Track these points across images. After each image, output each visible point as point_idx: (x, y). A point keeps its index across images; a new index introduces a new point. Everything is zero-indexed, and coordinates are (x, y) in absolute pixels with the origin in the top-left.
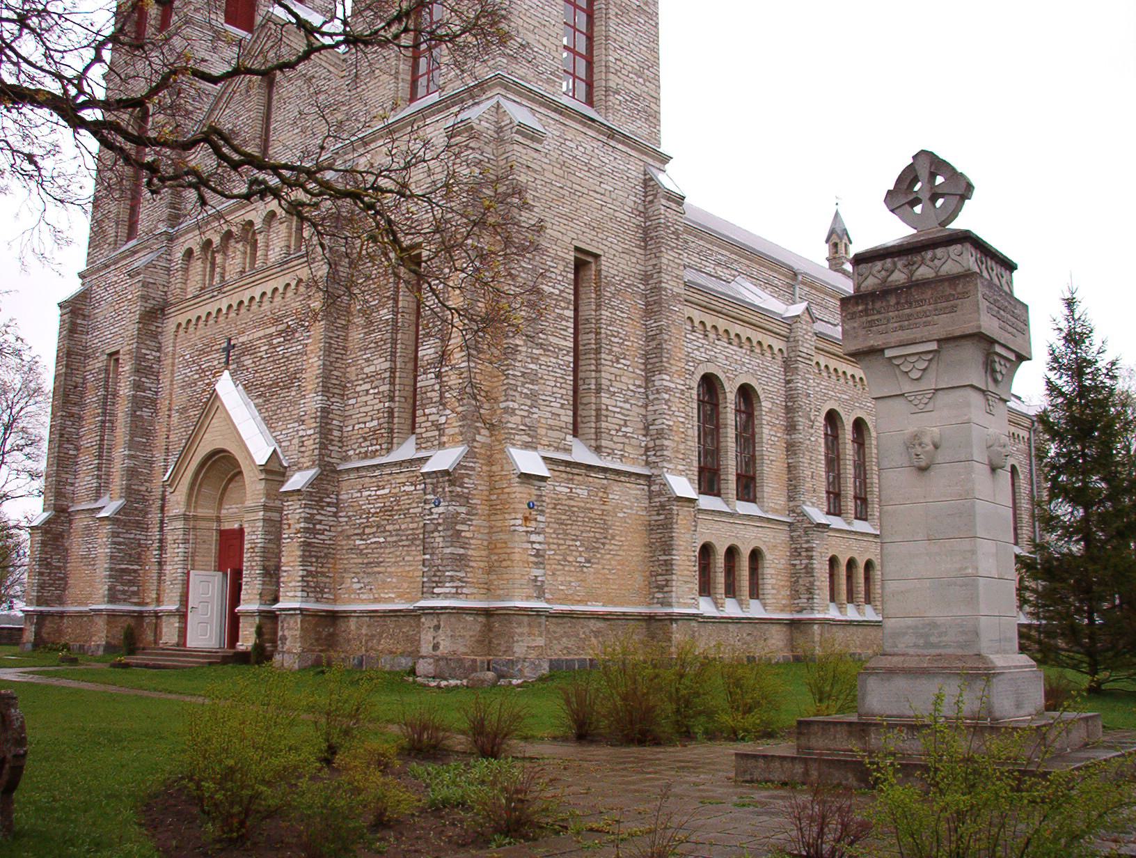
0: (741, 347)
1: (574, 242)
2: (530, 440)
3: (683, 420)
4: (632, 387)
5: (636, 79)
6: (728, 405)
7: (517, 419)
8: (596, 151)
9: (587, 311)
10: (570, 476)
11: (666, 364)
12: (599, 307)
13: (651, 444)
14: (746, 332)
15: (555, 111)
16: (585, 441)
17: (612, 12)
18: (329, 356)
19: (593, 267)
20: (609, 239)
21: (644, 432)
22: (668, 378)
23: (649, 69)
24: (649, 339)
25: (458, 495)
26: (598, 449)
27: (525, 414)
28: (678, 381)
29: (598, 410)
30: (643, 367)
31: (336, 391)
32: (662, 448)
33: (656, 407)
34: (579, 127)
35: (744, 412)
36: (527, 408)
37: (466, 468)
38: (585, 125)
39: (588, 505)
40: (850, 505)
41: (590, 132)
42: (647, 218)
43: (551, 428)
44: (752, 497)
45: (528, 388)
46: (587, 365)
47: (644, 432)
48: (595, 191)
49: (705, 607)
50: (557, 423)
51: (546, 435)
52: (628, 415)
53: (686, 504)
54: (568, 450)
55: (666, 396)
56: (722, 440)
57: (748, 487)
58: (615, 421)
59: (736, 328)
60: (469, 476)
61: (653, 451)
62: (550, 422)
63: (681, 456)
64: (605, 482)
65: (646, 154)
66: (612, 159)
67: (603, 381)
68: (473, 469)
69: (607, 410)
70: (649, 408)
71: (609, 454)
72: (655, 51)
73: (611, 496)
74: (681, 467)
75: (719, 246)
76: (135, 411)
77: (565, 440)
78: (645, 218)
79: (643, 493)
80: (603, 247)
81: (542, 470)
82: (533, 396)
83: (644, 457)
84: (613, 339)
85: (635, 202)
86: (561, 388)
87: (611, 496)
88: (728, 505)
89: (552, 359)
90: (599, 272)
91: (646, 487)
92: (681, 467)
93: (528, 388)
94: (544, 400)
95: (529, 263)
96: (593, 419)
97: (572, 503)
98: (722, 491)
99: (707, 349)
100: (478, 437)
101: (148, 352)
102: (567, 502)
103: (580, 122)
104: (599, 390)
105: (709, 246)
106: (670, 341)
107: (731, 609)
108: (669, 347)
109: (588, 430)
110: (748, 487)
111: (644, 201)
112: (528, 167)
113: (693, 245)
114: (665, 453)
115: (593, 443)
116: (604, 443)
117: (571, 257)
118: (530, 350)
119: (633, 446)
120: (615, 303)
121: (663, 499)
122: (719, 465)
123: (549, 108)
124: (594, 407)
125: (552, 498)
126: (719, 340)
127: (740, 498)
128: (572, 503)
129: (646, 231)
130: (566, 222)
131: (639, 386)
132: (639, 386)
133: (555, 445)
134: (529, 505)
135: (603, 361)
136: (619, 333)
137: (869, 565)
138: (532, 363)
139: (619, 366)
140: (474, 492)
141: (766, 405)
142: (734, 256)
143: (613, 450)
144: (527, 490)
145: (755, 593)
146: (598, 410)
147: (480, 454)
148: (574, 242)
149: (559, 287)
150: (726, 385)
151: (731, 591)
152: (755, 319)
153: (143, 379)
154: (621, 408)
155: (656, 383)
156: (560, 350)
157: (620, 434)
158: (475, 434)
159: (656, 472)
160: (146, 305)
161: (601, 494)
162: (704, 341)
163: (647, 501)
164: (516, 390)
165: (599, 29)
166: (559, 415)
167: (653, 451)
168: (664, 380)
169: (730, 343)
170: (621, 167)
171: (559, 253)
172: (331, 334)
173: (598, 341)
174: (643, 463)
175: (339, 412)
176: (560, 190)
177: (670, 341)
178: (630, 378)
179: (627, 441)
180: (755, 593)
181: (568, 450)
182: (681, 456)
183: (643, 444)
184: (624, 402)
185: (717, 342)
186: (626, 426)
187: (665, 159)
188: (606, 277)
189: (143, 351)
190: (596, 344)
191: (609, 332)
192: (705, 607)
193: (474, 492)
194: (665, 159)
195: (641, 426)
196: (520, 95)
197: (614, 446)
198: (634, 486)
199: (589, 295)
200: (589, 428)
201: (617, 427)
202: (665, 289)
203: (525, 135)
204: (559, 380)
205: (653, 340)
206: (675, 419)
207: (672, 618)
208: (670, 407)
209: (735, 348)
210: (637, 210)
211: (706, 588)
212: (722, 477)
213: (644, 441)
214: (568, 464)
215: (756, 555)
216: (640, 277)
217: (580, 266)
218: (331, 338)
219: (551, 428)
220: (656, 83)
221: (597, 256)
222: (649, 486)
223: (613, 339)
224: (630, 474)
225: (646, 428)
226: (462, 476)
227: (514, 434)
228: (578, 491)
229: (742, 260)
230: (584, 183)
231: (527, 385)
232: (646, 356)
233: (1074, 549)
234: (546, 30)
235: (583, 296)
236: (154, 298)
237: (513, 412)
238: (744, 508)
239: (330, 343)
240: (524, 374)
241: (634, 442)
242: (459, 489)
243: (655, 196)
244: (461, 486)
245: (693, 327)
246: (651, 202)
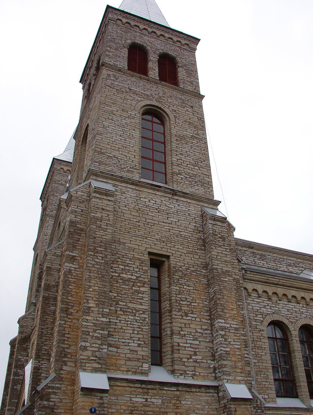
0: (299, 303)
1: (147, 250)
2: (100, 366)
3: (239, 347)
4: (199, 331)
5: (193, 167)
6: (294, 338)
8: (163, 202)
10: (146, 391)
11: (220, 313)
13: (217, 366)
14: (299, 294)
15: (132, 184)
17: (174, 140)
18: (41, 338)
19: (166, 263)
20: (176, 247)
21: (212, 358)
22: (223, 321)
25: (44, 407)
26: (173, 372)
27: (97, 349)
28: (232, 322)
30: (209, 318)
31: (44, 357)
32: (221, 366)
33: (217, 341)
34: (151, 191)
35: (306, 342)
36: (97, 346)
37: (53, 388)
38: (154, 190)
39: (162, 410)
41: (158, 193)
44: (295, 395)
45: (99, 333)
47: (212, 358)
48: (164, 222)
50: (135, 356)
51: (125, 364)
52: (196, 348)
53: (243, 403)
55: (223, 333)
56: (293, 360)
58: (185, 352)
59: (291, 293)
60: (55, 393)
62: (128, 356)
63: (239, 371)
64: (178, 393)
65: (202, 201)
66: (177, 205)
67: (174, 328)
68: (60, 388)
69: (179, 345)
70: (215, 342)
71: (181, 374)
73: (183, 402)
74: (239, 378)
75: (287, 256)
76: (13, 387)
77: (142, 367)
78: (204, 234)
79: (213, 398)
80: (171, 251)
83: (213, 374)
84: (181, 302)
85: (195, 226)
86: (138, 334)
87: (183, 402)
88: (304, 403)
89: (130, 317)
90: (169, 265)
91: (215, 395)
92: (239, 378)
93: (99, 333)
94: (123, 342)
95: (102, 260)
96: (170, 353)
97: (148, 409)
98: (299, 394)
99: (271, 307)
100: (64, 368)
101: (22, 357)
102: (143, 409)
103: (151, 189)
105: (281, 257)
106: (223, 298)
108: (222, 302)
109: (167, 360)
111: (202, 225)
112: (104, 209)
113: (269, 257)
114: (225, 369)
115: (170, 368)
116: (176, 367)
117: (146, 257)
118: (101, 310)
119: (203, 368)
121: (225, 401)
122: (294, 377)
123: (127, 183)
124: (169, 345)
125: (129, 406)
126: (280, 300)
128: (148, 409)
130: (142, 239)
131: (206, 330)
132: (206, 330)
133: (134, 370)
134: (91, 410)
135: (174, 316)
136: (186, 298)
138: (103, 317)
139: (188, 318)
140: (59, 404)
142: (299, 260)
143: (185, 371)
144: (90, 400)
147: (66, 378)
148: (147, 250)
149: (136, 275)
150: (291, 327)
152: (305, 286)
153: (18, 371)
154: (191, 344)
155: (216, 326)
156: (137, 311)
157: (191, 360)
158: (62, 365)
159: (220, 383)
160: (22, 335)
161: (174, 402)
162: (268, 302)
163: (218, 404)
164: (89, 335)
166: (136, 351)
169: (290, 302)
170: (183, 209)
171: (135, 256)
172: (43, 327)
173: (171, 305)
174: (213, 378)
175: (46, 369)
176: (137, 223)
177: (223, 298)
178: (197, 325)
179: (198, 365)
182: (239, 371)
183: (212, 366)
184: (193, 340)
185: (278, 302)
186: (195, 354)
187: (218, 203)
188: (174, 267)
189: (19, 357)
190: (170, 307)
191: (178, 299)
193: (59, 404)
194: (218, 203)
195: (210, 354)
196: (107, 178)
197: (186, 369)
198: (204, 394)
201: (189, 356)
202: (216, 269)
203: (100, 193)
204: (136, 329)
205: (212, 300)
206: (231, 346)
208: (226, 340)
209: (294, 304)
210: (197, 230)
212: (297, 385)
213: (212, 364)
216: (202, 266)
218: (43, 329)
220: (208, 168)
222: (218, 393)
223: (181, 302)
224: (200, 387)
225: (213, 356)
226: (49, 394)
227: (85, 363)
228: (153, 400)
229: (305, 261)
230: (154, 218)
231: (98, 331)
232: (210, 311)
234: (127, 149)
235: (162, 281)
236: (26, 333)
239: (42, 332)
240: (95, 325)
241: (202, 365)
242: (45, 403)
243: (206, 220)
244: (48, 400)
245: (258, 294)
246: (205, 224)
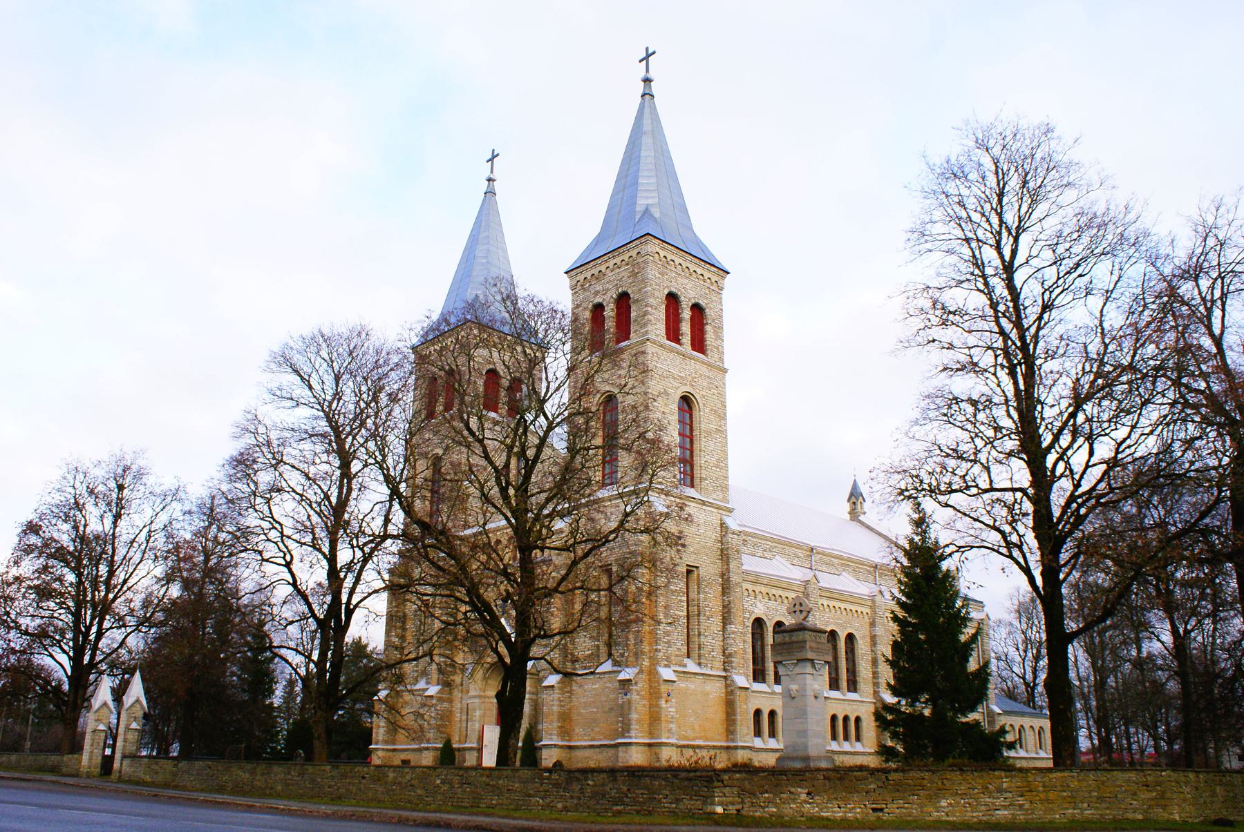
7: (661, 654)
9: (693, 595)
12: (699, 593)
16: (694, 660)
23: (722, 464)
24: (724, 607)
26: (700, 664)
29: (699, 645)
32: (731, 662)
40: (844, 683)
42: (722, 544)
43: (677, 656)
46: (694, 621)
49: (834, 746)
54: (685, 666)
57: (853, 686)
61: (727, 664)
72: (725, 452)
81: (673, 677)
82: (668, 643)
90: (699, 575)
104: (699, 635)
107: (847, 747)
110: (853, 686)
120: (707, 590)
127: (849, 690)
129: (722, 550)
137: (772, 714)
141: (860, 641)
145: (858, 739)
146: (699, 645)
151: (846, 738)
152: (834, 596)
165: (696, 446)
167: (727, 664)
168: (731, 628)
173: (699, 611)
180: (858, 739)
181: (685, 666)
192: (758, 743)
199: (694, 587)
200: (695, 654)
207: (736, 748)
211: (758, 733)
214: (684, 672)
215: (858, 719)
217: (689, 572)
219: (677, 656)
221: (697, 567)
225: (724, 652)
233: (489, 660)
237: (660, 651)
238: (851, 696)
